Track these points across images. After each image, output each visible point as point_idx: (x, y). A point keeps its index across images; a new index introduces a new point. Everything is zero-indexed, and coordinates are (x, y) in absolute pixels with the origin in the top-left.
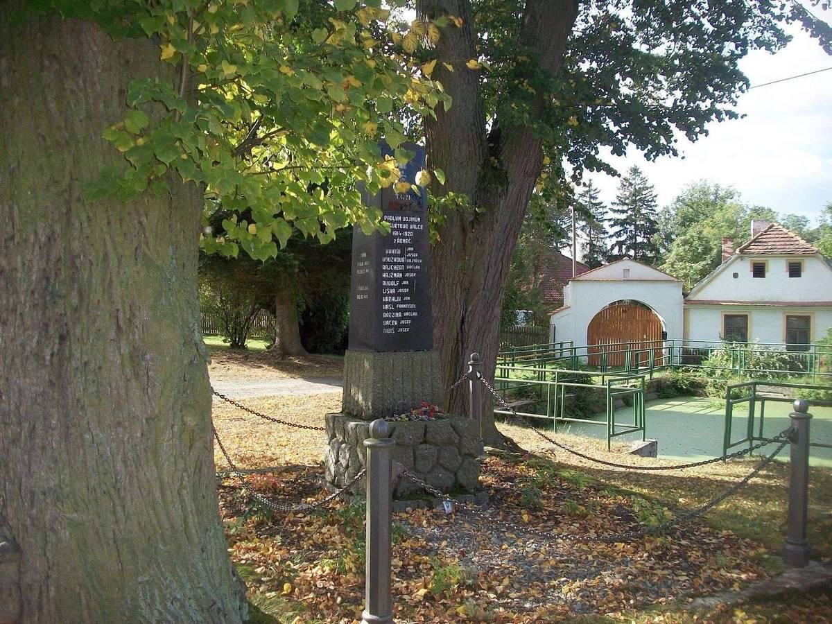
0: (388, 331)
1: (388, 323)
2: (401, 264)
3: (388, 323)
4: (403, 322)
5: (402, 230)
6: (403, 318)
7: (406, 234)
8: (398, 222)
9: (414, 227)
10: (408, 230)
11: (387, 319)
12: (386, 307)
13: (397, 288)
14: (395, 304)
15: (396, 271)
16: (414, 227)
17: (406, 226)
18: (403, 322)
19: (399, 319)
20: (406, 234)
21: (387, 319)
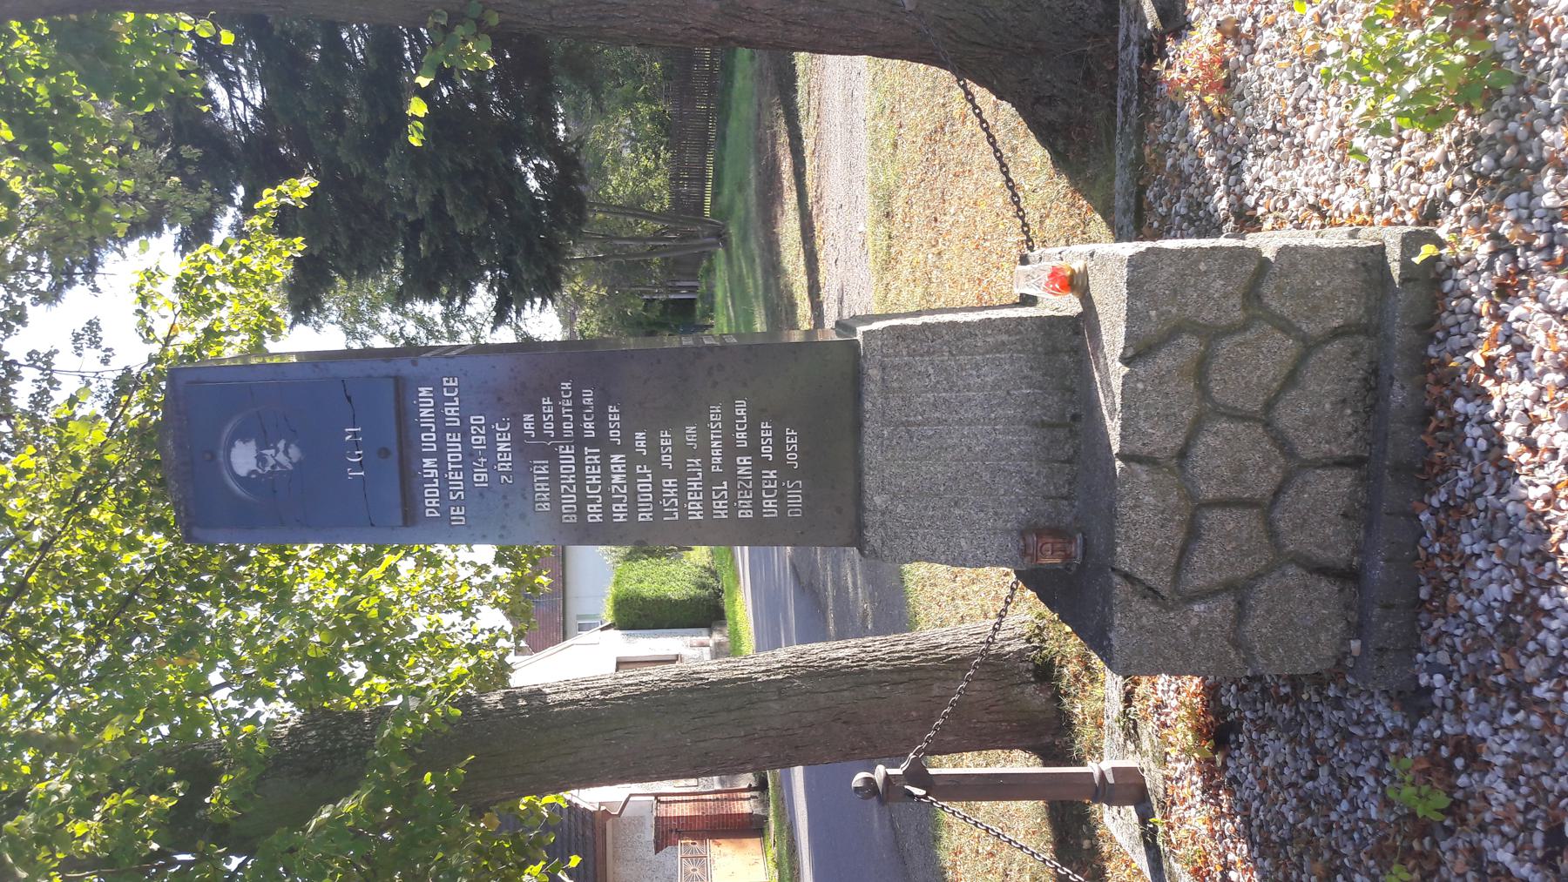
0: (795, 499)
1: (769, 504)
2: (605, 463)
3: (769, 504)
4: (767, 451)
5: (469, 454)
6: (754, 449)
7: (478, 441)
8: (442, 466)
9: (451, 411)
10: (465, 431)
11: (757, 504)
12: (720, 509)
13: (660, 473)
14: (710, 480)
15: (606, 476)
16: (451, 411)
17: (454, 440)
18: (767, 451)
19: (759, 464)
20: (478, 441)
21: (757, 504)
